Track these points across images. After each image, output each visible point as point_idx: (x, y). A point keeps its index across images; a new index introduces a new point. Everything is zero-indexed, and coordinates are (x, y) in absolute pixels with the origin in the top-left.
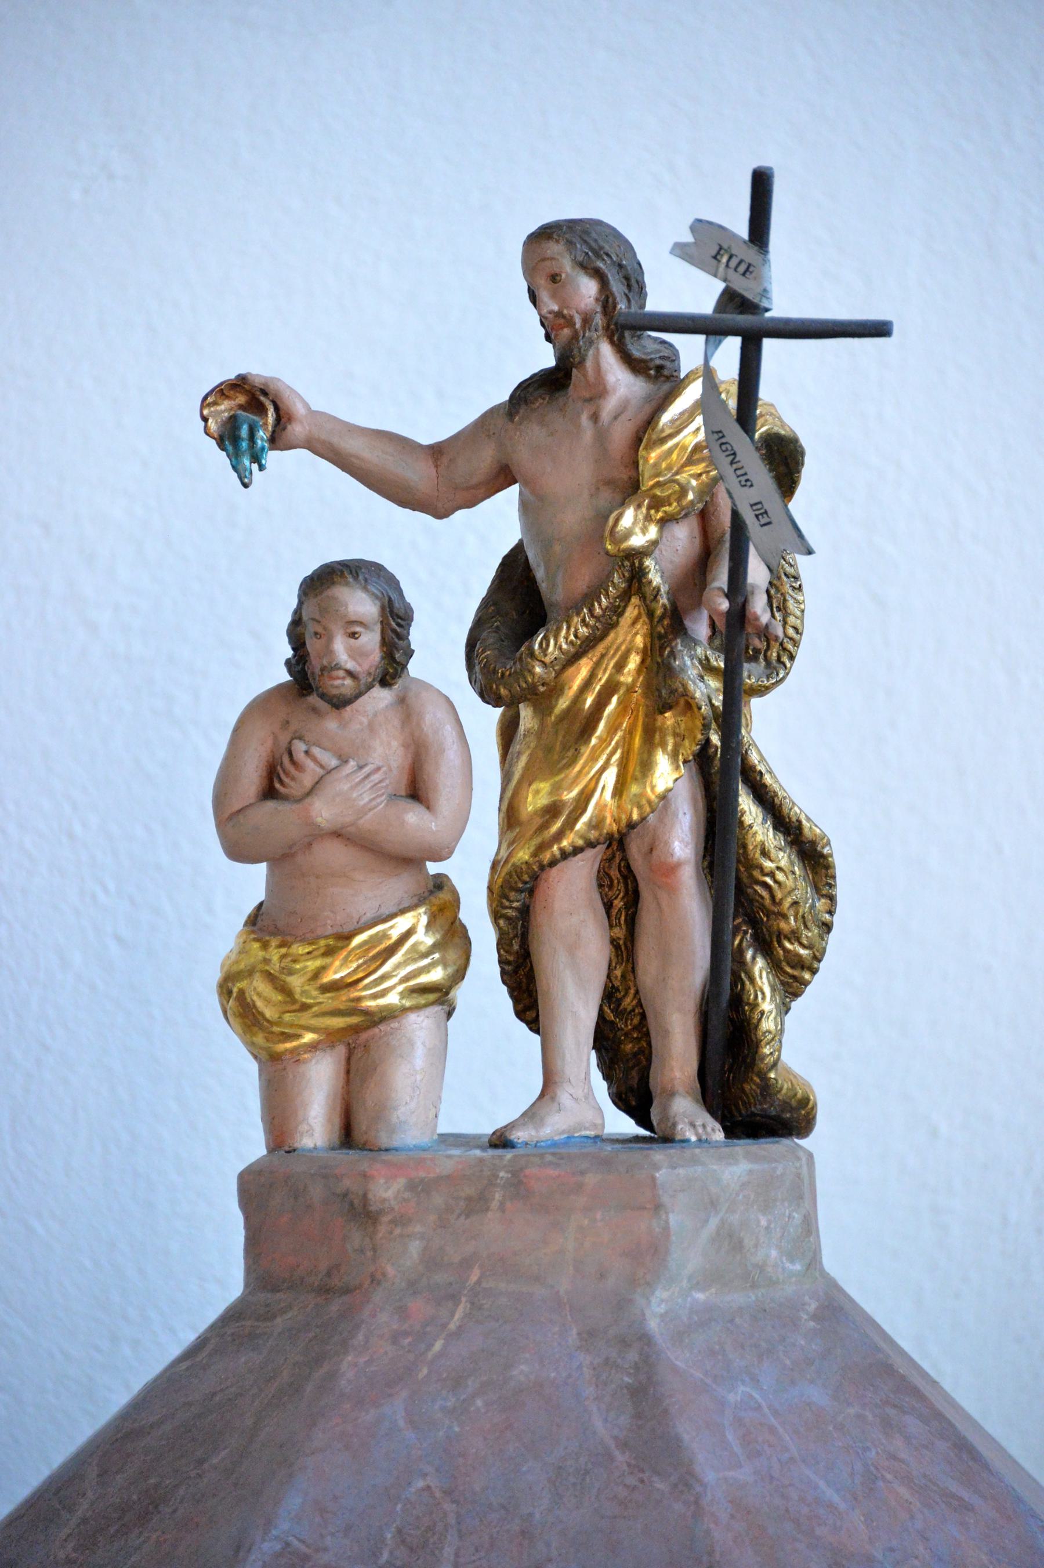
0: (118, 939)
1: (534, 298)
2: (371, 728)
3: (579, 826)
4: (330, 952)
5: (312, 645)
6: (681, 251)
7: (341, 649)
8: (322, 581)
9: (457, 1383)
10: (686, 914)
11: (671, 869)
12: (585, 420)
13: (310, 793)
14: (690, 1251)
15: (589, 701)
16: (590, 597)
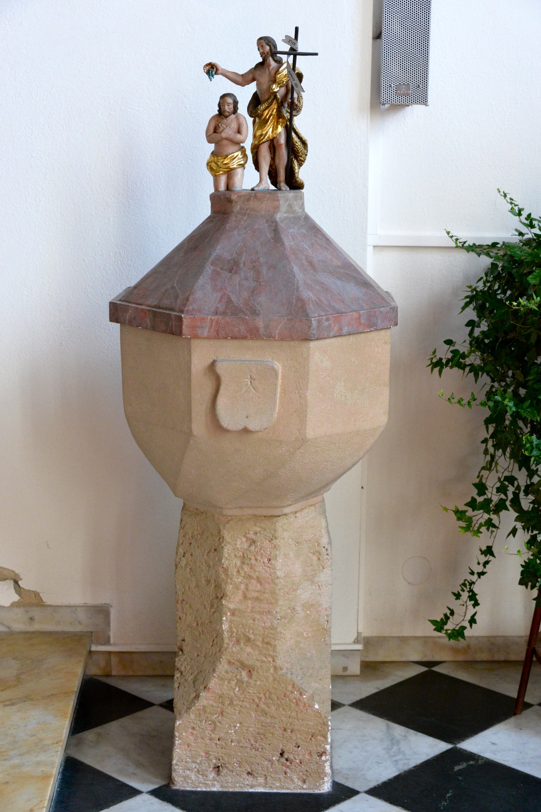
0: (190, 159)
1: (259, 50)
2: (232, 121)
3: (266, 138)
4: (225, 158)
5: (222, 107)
6: (283, 40)
7: (227, 108)
8: (223, 97)
9: (245, 228)
10: (283, 153)
11: (281, 145)
12: (267, 70)
13: (222, 132)
14: (284, 207)
15: (268, 117)
16: (268, 100)
